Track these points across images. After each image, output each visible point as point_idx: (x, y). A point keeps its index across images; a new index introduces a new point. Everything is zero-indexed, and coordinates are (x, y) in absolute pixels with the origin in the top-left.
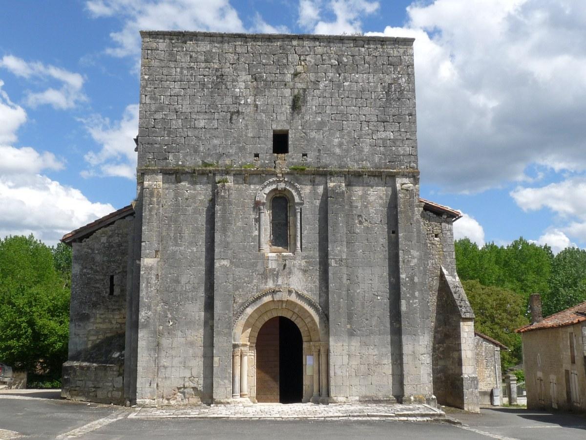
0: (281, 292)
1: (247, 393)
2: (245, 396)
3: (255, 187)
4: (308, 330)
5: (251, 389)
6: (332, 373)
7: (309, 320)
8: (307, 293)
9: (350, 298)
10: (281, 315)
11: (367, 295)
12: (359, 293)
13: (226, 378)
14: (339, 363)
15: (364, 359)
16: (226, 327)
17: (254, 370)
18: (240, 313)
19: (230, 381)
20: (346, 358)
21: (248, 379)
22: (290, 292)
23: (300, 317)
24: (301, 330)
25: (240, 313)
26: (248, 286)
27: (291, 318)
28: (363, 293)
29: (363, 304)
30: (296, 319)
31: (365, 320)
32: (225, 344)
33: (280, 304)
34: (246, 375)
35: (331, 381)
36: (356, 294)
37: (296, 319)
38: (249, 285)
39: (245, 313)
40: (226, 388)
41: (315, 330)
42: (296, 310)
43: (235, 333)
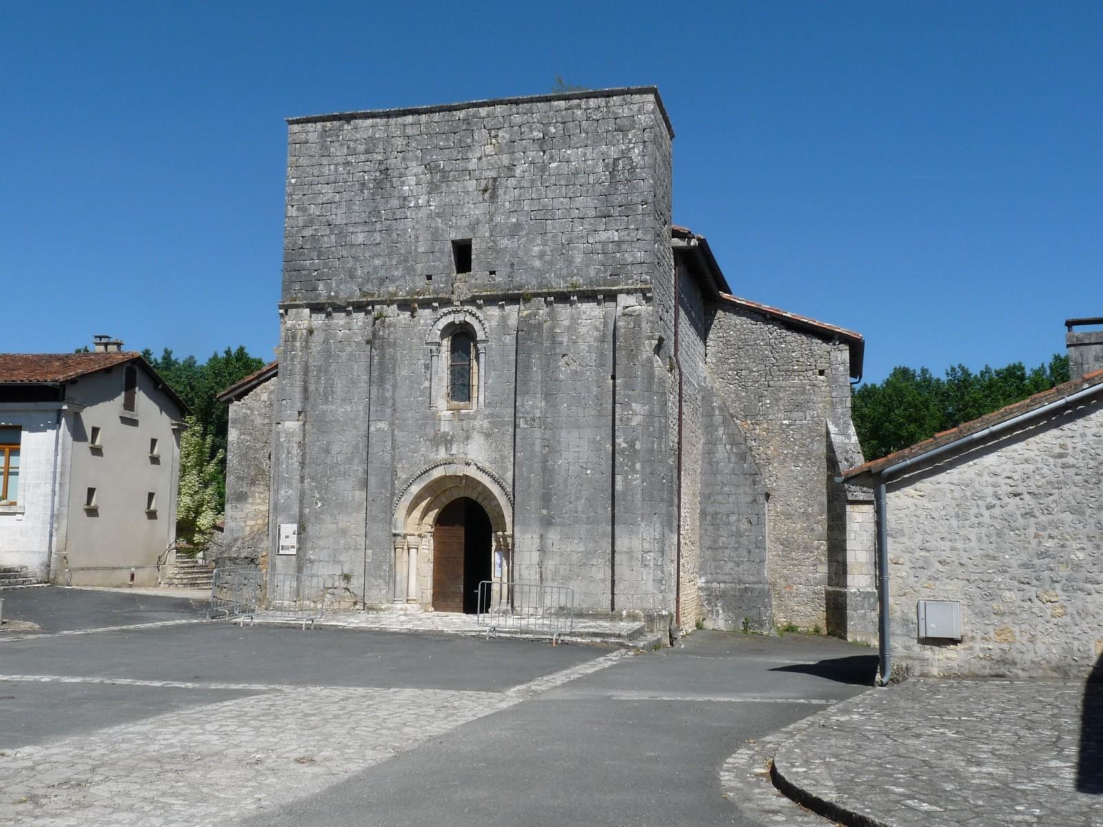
11: (571, 468)
12: (561, 465)
13: (380, 577)
14: (526, 562)
17: (428, 569)
26: (413, 457)
32: (380, 533)
36: (556, 467)
38: (415, 455)
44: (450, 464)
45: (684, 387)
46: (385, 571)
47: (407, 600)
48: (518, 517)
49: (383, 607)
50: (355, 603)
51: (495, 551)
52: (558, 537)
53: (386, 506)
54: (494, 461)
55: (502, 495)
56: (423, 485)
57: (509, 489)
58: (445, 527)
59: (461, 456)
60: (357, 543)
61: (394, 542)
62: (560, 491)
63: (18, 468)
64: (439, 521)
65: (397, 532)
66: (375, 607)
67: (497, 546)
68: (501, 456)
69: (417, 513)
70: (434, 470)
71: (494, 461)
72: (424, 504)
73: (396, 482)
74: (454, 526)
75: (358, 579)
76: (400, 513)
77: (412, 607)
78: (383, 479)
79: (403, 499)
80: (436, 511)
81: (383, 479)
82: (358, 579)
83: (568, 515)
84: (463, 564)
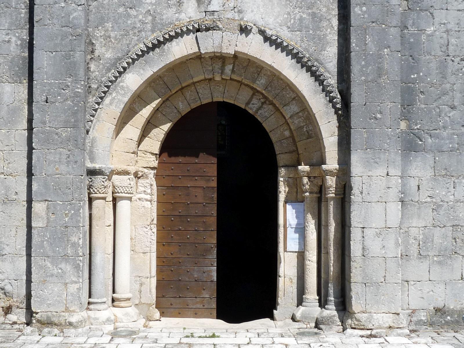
0: (220, 29)
1: (129, 295)
2: (122, 304)
3: (330, 173)
4: (292, 137)
5: (141, 285)
6: (355, 248)
7: (294, 108)
8: (289, 35)
9: (411, 52)
10: (221, 100)
11: (453, 41)
12: (431, 35)
13: (65, 258)
14: (377, 222)
15: (442, 213)
16: (67, 122)
17: (150, 238)
18: (108, 87)
19: (77, 267)
20: (395, 209)
21: (132, 259)
22: (244, 30)
23: (272, 103)
24: (274, 137)
25: (108, 87)
26: (129, 16)
27: (248, 104)
28: (445, 35)
29: (443, 66)
30: (259, 108)
31: (447, 109)
32: (63, 168)
33: (217, 66)
34: (128, 248)
35: (353, 270)
36: (423, 38)
37: (259, 108)
38: (133, 12)
39: (122, 88)
40: (66, 284)
41: (309, 137)
42: (260, 84)
43: (93, 141)
44: (207, 29)
45: (144, 102)
46: (74, 245)
47: (113, 300)
48: (357, 136)
49: (74, 319)
50: (8, 310)
51: (286, 202)
52: (430, 173)
53: (75, 113)
54: (299, 27)
55: (316, 92)
56: (149, 72)
57: (332, 81)
58: (181, 159)
59: (230, 15)
60: (7, 189)
61: (90, 187)
62: (432, 85)
63: (338, 292)
64: (168, 147)
65: (97, 166)
66: (55, 320)
67: (288, 194)
68: (314, 15)
69: (132, 130)
70: (175, 42)
71: (299, 27)
72: (146, 112)
73: (93, 67)
74: (197, 156)
75: (13, 262)
76: (103, 126)
77: (127, 314)
78: (67, 57)
79: (107, 100)
80: (166, 127)
81: (67, 57)
82: (13, 262)
83: (449, 131)
84: (214, 227)
